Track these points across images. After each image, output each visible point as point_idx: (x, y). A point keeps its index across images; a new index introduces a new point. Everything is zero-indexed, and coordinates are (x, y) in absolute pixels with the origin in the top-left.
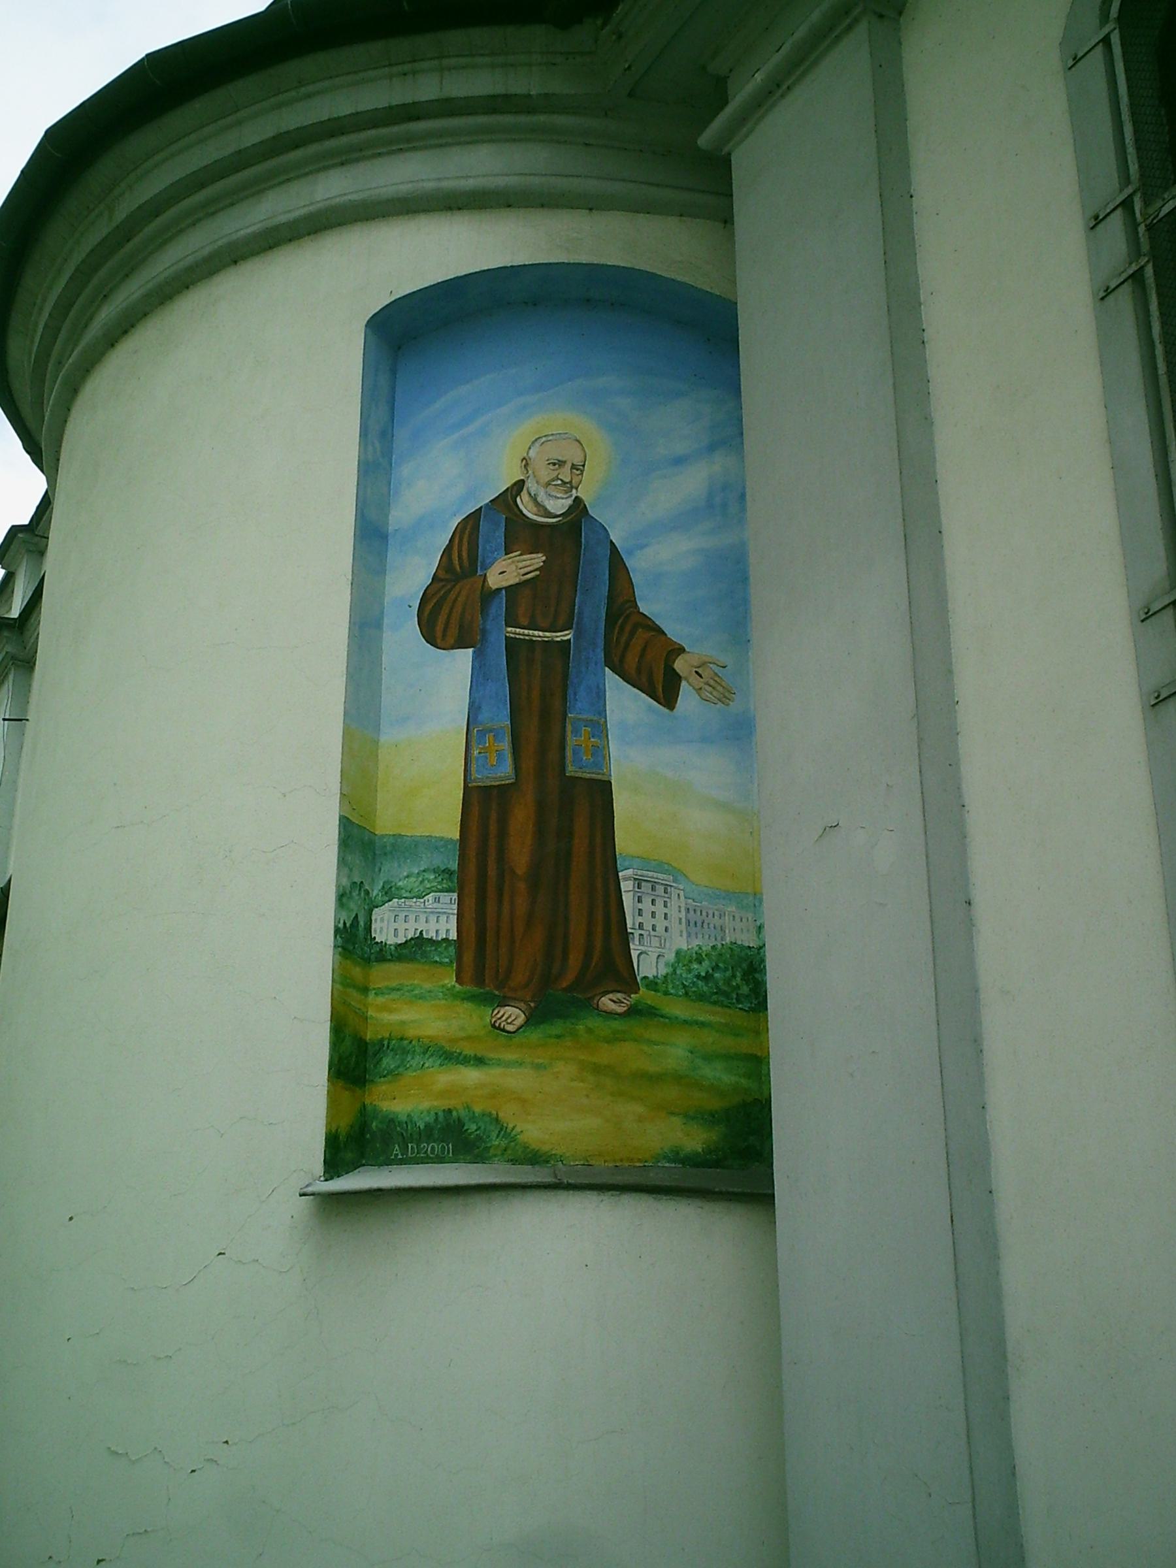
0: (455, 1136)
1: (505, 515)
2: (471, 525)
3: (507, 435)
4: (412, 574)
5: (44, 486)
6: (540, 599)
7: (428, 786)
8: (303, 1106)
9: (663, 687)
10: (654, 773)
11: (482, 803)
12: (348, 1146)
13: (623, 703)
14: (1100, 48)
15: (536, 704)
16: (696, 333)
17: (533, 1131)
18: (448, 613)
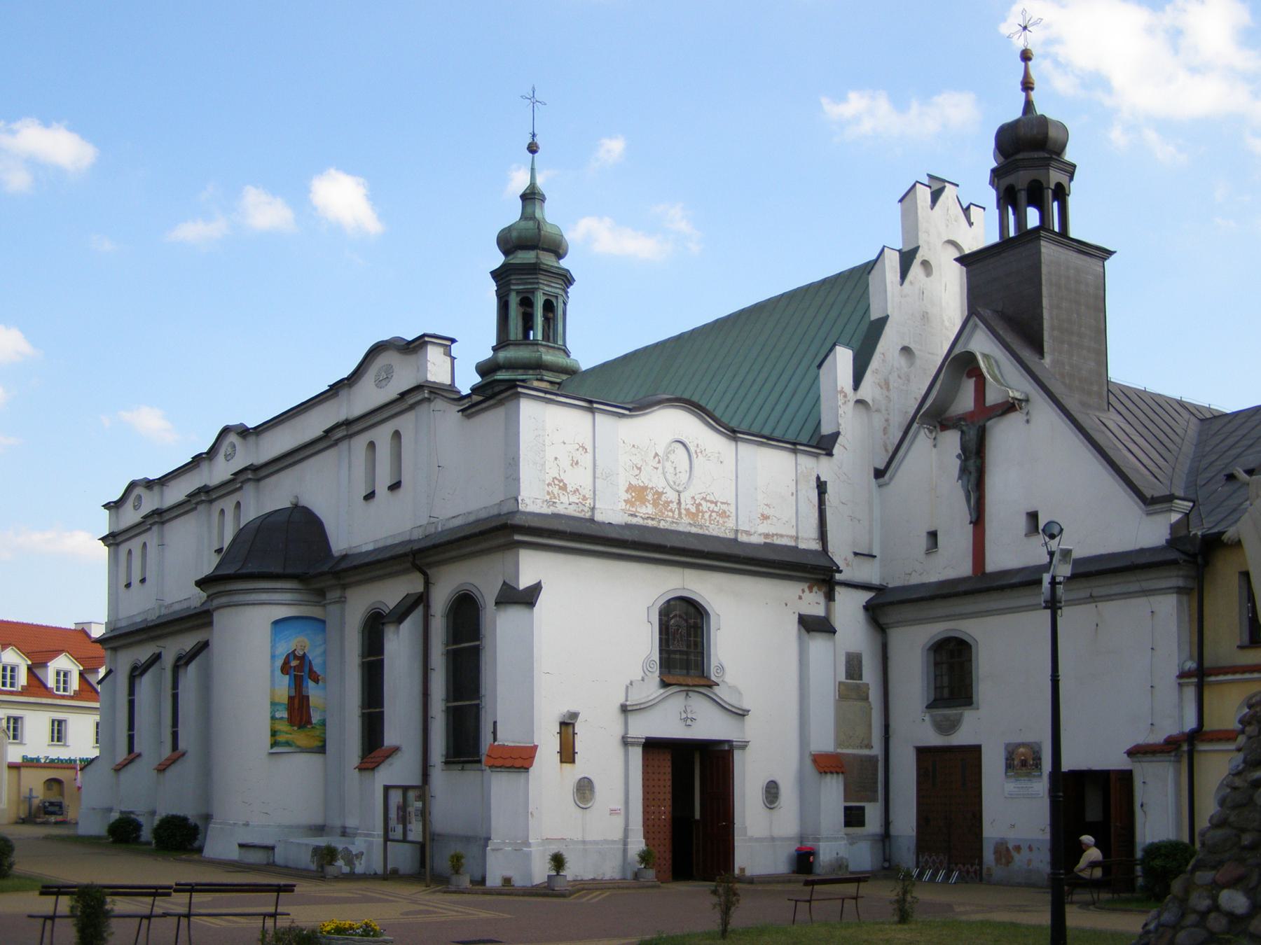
2: (288, 656)
3: (293, 642)
4: (279, 663)
8: (267, 740)
9: (317, 681)
10: (312, 690)
11: (291, 698)
12: (274, 744)
13: (311, 684)
14: (809, 542)
15: (298, 683)
17: (299, 743)
18: (285, 669)
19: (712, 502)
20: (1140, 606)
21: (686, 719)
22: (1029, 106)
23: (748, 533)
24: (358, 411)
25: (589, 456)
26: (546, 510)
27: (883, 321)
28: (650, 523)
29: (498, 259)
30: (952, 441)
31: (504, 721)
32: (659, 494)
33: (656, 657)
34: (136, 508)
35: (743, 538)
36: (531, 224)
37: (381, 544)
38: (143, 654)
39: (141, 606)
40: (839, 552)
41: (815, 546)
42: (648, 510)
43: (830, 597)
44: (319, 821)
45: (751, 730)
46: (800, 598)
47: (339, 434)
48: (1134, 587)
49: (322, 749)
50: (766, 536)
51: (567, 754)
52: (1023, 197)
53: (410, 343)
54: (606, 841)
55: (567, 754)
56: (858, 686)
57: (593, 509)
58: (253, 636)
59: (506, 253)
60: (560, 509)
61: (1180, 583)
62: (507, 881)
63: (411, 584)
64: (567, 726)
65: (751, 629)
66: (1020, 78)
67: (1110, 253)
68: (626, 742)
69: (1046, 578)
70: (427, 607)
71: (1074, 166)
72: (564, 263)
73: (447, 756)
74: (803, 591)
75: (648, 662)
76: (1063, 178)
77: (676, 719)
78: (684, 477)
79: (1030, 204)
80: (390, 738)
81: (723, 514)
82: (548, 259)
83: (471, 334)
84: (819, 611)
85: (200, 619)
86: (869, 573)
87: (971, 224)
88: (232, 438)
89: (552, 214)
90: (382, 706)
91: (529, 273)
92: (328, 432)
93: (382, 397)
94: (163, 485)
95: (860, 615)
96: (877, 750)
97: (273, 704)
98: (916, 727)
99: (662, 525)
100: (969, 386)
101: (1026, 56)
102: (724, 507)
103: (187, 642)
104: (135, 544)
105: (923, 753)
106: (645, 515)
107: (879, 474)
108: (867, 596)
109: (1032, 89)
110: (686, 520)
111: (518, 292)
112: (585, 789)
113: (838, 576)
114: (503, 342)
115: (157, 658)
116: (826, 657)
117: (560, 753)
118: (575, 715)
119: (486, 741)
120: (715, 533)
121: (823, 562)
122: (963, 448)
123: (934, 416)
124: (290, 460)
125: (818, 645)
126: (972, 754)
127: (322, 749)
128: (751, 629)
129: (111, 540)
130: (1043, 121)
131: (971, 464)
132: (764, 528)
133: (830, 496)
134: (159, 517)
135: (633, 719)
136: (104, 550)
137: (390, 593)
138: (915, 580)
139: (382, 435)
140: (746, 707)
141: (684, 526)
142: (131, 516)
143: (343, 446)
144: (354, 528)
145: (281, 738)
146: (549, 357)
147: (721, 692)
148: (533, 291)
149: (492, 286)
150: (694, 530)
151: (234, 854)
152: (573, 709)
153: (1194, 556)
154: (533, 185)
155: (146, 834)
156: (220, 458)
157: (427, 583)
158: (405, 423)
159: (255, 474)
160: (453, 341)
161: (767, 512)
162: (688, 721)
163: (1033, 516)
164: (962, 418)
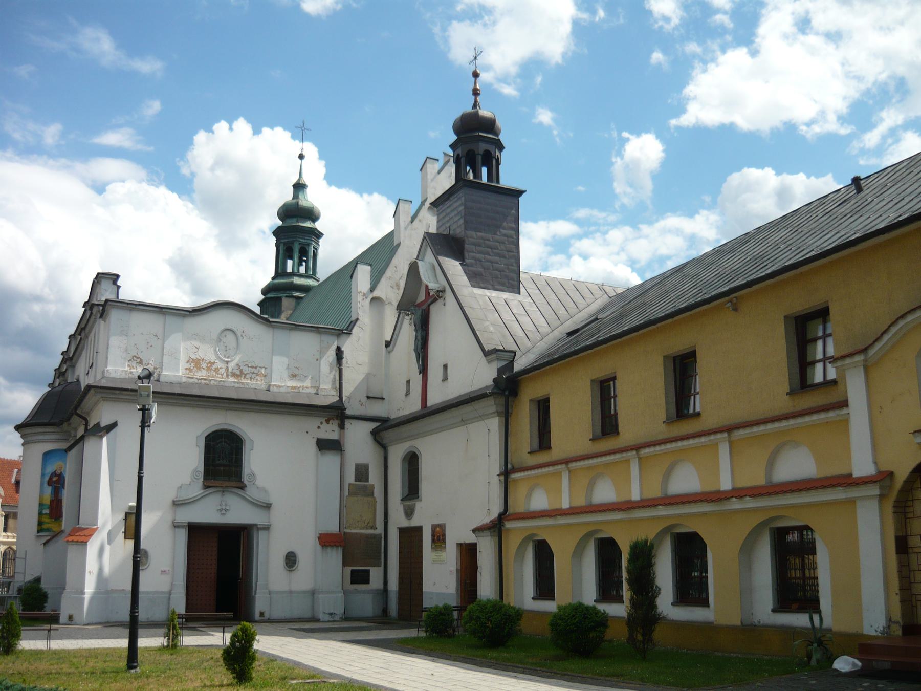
1: (54, 474)
4: (47, 478)
6: (57, 482)
11: (52, 501)
19: (252, 367)
27: (399, 245)
33: (202, 469)
42: (202, 374)
43: (342, 427)
45: (277, 518)
46: (319, 427)
52: (479, 159)
56: (365, 486)
67: (520, 193)
68: (176, 526)
74: (321, 423)
75: (196, 471)
77: (210, 511)
79: (483, 165)
84: (335, 436)
86: (377, 410)
95: (369, 439)
96: (380, 530)
97: (41, 505)
105: (402, 531)
107: (388, 344)
108: (373, 425)
109: (479, 94)
125: (331, 460)
126: (419, 530)
145: (44, 527)
147: (251, 492)
148: (293, 243)
161: (296, 372)
162: (223, 511)
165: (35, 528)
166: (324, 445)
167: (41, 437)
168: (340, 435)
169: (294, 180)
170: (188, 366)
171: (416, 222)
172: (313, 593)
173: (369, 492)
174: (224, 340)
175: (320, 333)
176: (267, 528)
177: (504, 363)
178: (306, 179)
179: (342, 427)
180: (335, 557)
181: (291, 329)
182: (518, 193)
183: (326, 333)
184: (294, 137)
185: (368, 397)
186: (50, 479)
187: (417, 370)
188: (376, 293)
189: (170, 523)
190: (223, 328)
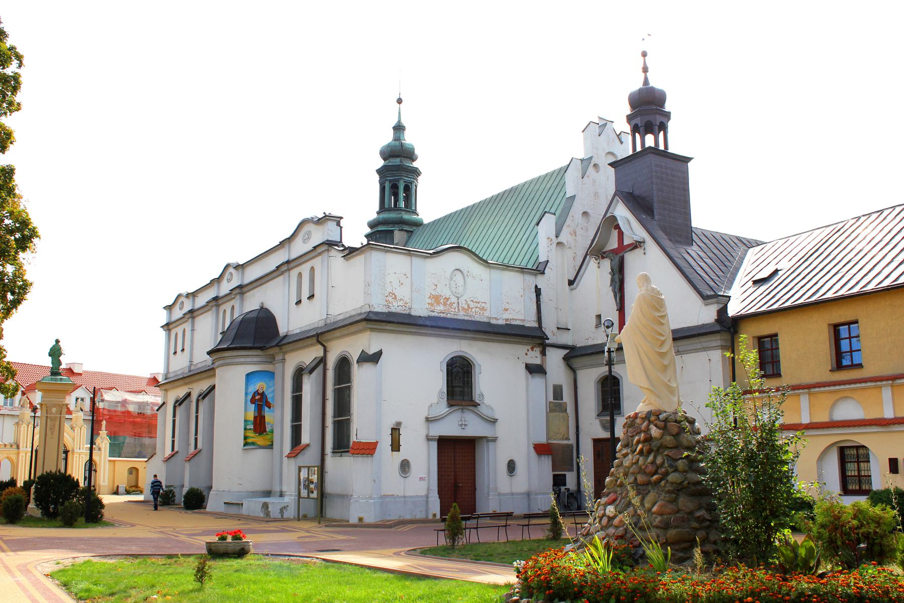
0: (253, 444)
1: (257, 393)
4: (250, 397)
5: (359, 246)
6: (260, 400)
7: (251, 416)
11: (255, 418)
12: (246, 444)
13: (266, 409)
14: (531, 322)
15: (259, 409)
16: (271, 375)
18: (253, 401)
20: (702, 356)
21: (461, 425)
22: (646, 82)
23: (496, 319)
24: (294, 255)
25: (409, 280)
26: (385, 310)
28: (442, 315)
29: (381, 163)
30: (606, 264)
31: (361, 429)
32: (448, 299)
33: (445, 390)
34: (181, 309)
35: (494, 322)
36: (397, 143)
37: (303, 330)
38: (181, 392)
39: (180, 364)
40: (549, 327)
41: (536, 325)
42: (441, 308)
43: (543, 353)
44: (266, 488)
45: (500, 431)
47: (284, 268)
48: (699, 346)
49: (271, 446)
50: (507, 320)
51: (396, 446)
53: (320, 219)
54: (417, 496)
55: (396, 446)
57: (410, 309)
58: (233, 384)
59: (385, 159)
60: (393, 310)
61: (719, 343)
62: (361, 519)
63: (316, 352)
64: (395, 431)
65: (499, 375)
66: (642, 65)
67: (689, 159)
68: (429, 439)
69: (606, 349)
70: (325, 365)
71: (670, 113)
72: (415, 164)
73: (334, 448)
75: (441, 392)
76: (663, 119)
77: (454, 426)
78: (461, 290)
80: (305, 439)
81: (483, 309)
82: (407, 163)
83: (359, 210)
84: (538, 361)
85: (209, 372)
86: (566, 339)
87: (622, 143)
88: (231, 270)
89: (409, 138)
90: (301, 421)
91: (398, 172)
92: (278, 267)
93: (314, 244)
94: (290, 243)
96: (572, 441)
98: (593, 428)
99: (449, 316)
100: (615, 233)
101: (644, 54)
102: (483, 305)
103: (204, 386)
104: (179, 330)
105: (596, 442)
106: (439, 310)
107: (571, 283)
110: (462, 313)
111: (390, 181)
112: (405, 466)
113: (547, 341)
114: (383, 208)
115: (188, 395)
116: (540, 389)
117: (391, 445)
118: (399, 424)
119: (353, 438)
120: (478, 319)
121: (539, 334)
122: (612, 269)
123: (597, 251)
124: (258, 283)
125: (537, 382)
127: (271, 446)
128: (499, 375)
129: (167, 327)
130: (653, 89)
131: (617, 277)
132: (506, 316)
133: (543, 297)
134: (192, 314)
135: (432, 425)
136: (163, 333)
137: (308, 355)
138: (590, 343)
139: (305, 269)
140: (496, 417)
141: (461, 316)
142: (178, 313)
143: (286, 274)
144: (291, 321)
146: (406, 216)
147: (482, 409)
148: (398, 180)
149: (377, 177)
150: (466, 318)
151: (222, 508)
152: (399, 420)
153: (729, 328)
154: (399, 121)
155: (180, 498)
156: (225, 282)
157: (325, 351)
158: (317, 262)
159: (241, 290)
160: (341, 218)
161: (507, 306)
162: (463, 426)
163: (599, 317)
164: (613, 251)
165: (242, 442)
166: (535, 370)
167: (242, 360)
168: (542, 361)
169: (394, 123)
170: (429, 301)
171: (585, 177)
172: (528, 494)
173: (562, 408)
174: (454, 278)
175: (523, 272)
176: (494, 440)
177: (721, 306)
178: (404, 122)
179: (543, 353)
180: (547, 463)
181: (503, 269)
182: (687, 160)
183: (493, 268)
184: (629, 118)
185: (558, 328)
186: (254, 397)
187: (615, 308)
188: (560, 239)
189: (424, 437)
190: (454, 268)
